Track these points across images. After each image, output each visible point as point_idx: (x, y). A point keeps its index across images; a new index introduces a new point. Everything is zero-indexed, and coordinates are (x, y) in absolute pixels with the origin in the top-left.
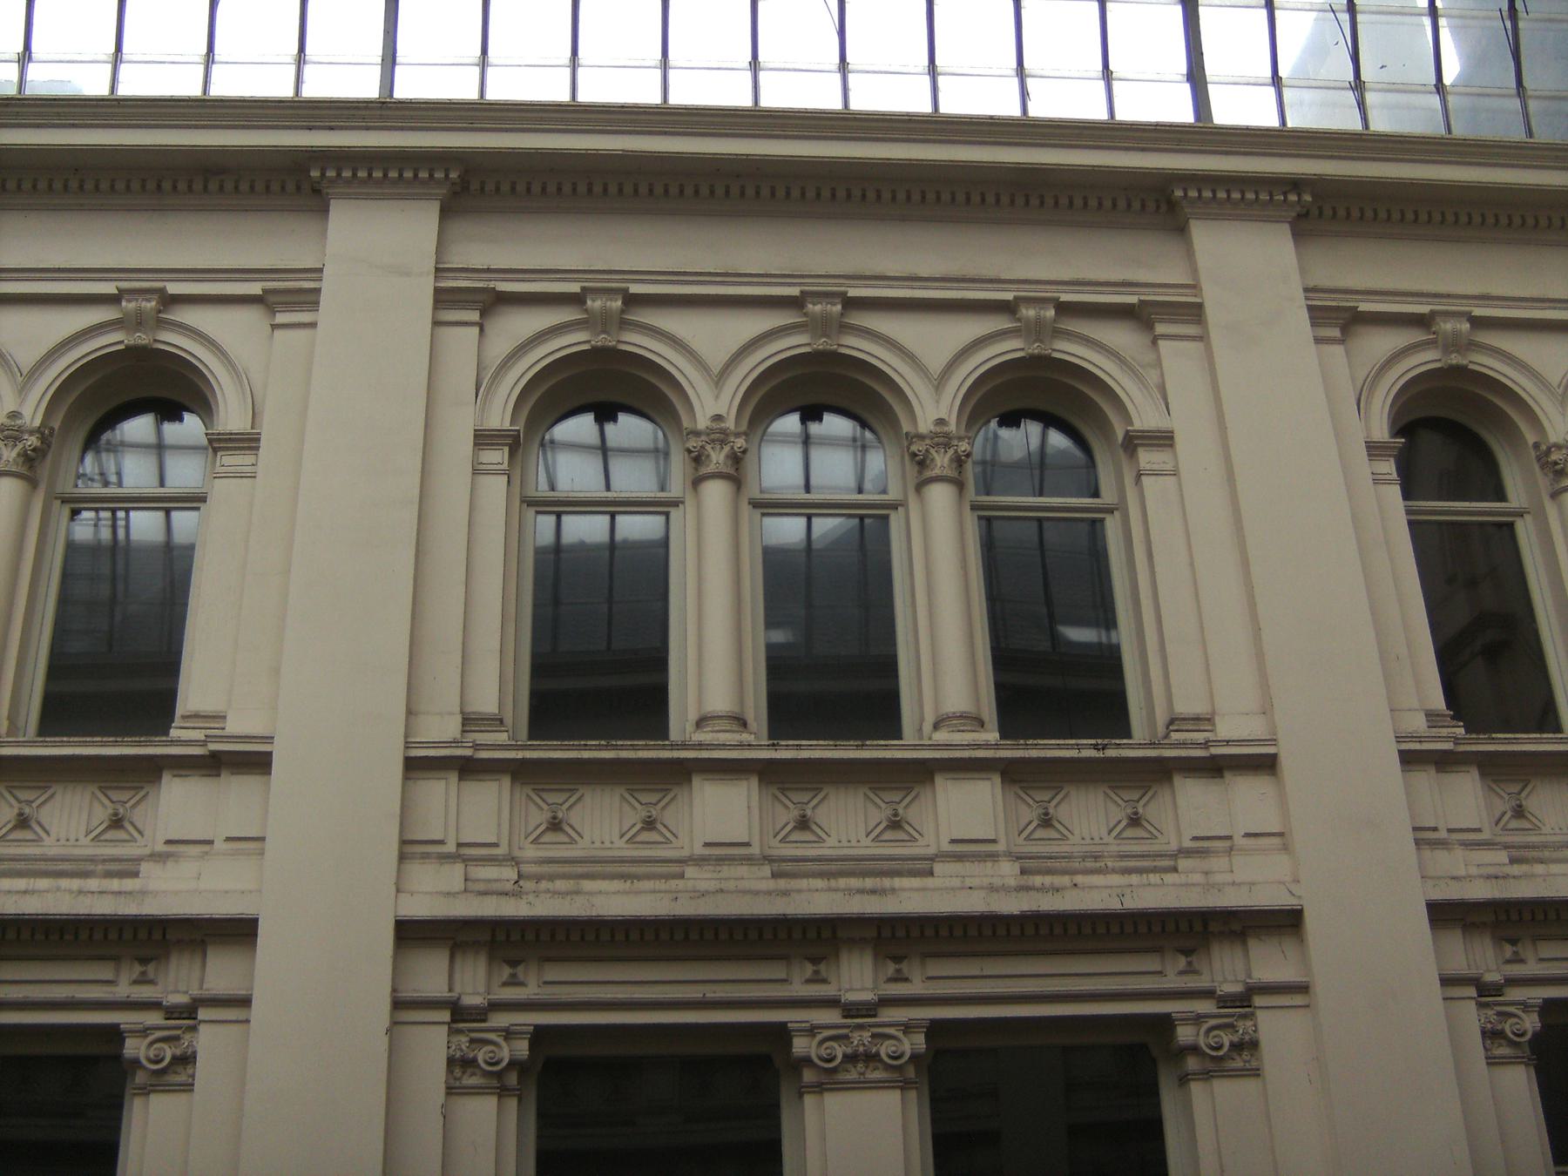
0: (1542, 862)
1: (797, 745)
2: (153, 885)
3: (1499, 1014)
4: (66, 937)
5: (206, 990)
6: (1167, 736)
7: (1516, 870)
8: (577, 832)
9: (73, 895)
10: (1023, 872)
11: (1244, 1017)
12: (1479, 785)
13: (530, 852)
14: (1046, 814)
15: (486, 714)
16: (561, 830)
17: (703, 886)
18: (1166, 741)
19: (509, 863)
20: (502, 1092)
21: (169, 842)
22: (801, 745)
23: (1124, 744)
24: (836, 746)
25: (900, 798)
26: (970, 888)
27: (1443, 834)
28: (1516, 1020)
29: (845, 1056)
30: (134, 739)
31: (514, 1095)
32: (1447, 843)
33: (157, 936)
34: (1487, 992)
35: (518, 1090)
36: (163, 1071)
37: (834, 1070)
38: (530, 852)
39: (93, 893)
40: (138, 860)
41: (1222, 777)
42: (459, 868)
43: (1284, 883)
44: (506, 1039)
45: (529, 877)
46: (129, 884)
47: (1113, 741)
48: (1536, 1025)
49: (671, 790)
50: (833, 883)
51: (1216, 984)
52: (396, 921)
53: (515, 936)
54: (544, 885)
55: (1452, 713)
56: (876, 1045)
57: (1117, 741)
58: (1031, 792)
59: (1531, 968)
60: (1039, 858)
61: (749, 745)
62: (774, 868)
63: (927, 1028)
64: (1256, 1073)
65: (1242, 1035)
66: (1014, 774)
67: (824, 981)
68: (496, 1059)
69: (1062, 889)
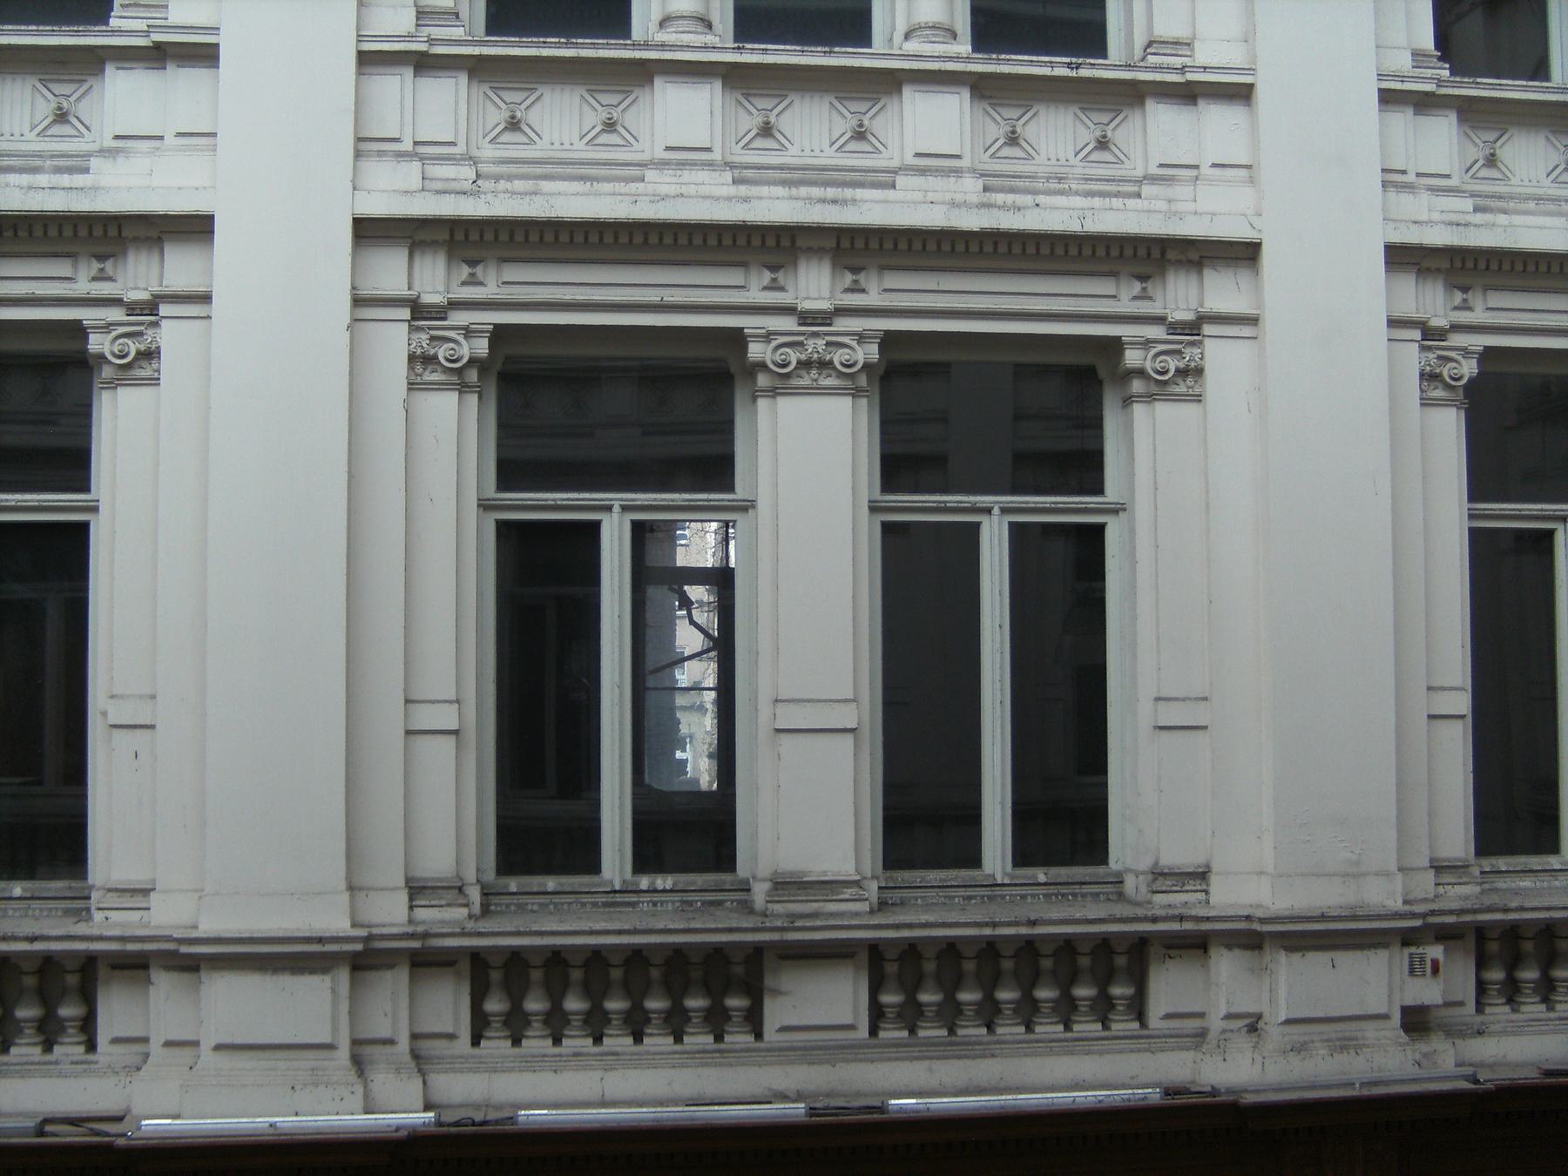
0: (1505, 212)
1: (763, 50)
2: (105, 181)
3: (1440, 358)
4: (20, 233)
5: (166, 287)
6: (1143, 59)
7: (1479, 218)
8: (536, 133)
9: (23, 191)
10: (986, 189)
11: (1193, 344)
12: (1455, 132)
13: (488, 152)
14: (1014, 132)
15: (442, 8)
16: (520, 129)
17: (664, 189)
18: (1142, 64)
19: (467, 163)
20: (463, 388)
21: (117, 137)
22: (766, 50)
23: (1098, 65)
24: (803, 51)
25: (867, 108)
26: (932, 203)
27: (1411, 178)
28: (1454, 365)
29: (799, 362)
30: (72, 28)
31: (476, 392)
32: (1413, 187)
33: (113, 232)
34: (1430, 334)
35: (478, 387)
36: (128, 366)
37: (788, 376)
38: (488, 152)
39: (44, 188)
40: (87, 155)
41: (1195, 104)
42: (416, 166)
43: (1246, 216)
44: (466, 337)
45: (488, 177)
46: (79, 180)
47: (1088, 61)
48: (1473, 371)
49: (632, 91)
50: (794, 191)
51: (1167, 311)
52: (354, 219)
53: (474, 236)
54: (502, 185)
55: (1439, 54)
56: (830, 353)
57: (1092, 61)
58: (1000, 109)
59: (1478, 316)
60: (1002, 176)
61: (714, 48)
62: (736, 175)
63: (882, 339)
64: (1198, 399)
65: (1188, 361)
66: (984, 88)
67: (782, 289)
68: (456, 357)
69: (1024, 208)
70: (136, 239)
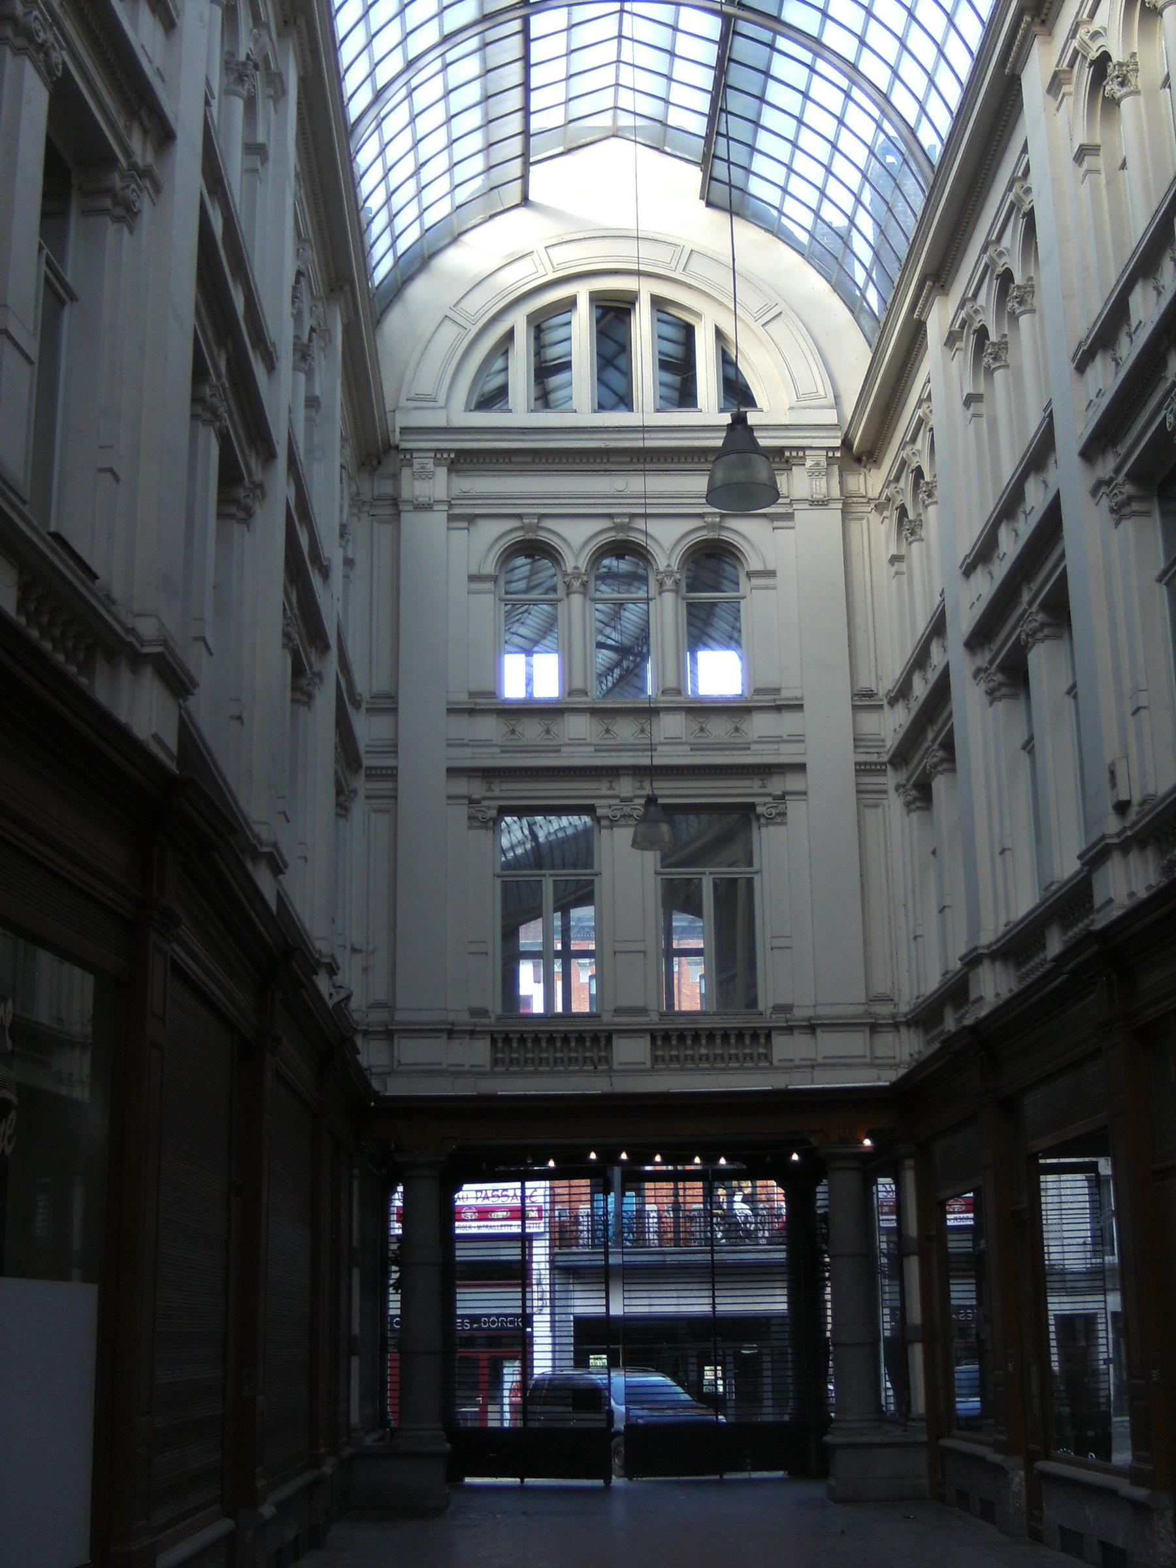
33: (767, 770)
70: (776, 773)
